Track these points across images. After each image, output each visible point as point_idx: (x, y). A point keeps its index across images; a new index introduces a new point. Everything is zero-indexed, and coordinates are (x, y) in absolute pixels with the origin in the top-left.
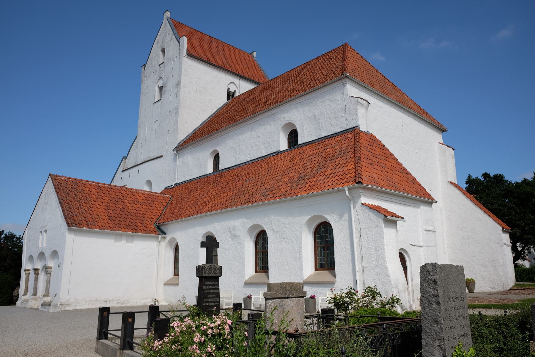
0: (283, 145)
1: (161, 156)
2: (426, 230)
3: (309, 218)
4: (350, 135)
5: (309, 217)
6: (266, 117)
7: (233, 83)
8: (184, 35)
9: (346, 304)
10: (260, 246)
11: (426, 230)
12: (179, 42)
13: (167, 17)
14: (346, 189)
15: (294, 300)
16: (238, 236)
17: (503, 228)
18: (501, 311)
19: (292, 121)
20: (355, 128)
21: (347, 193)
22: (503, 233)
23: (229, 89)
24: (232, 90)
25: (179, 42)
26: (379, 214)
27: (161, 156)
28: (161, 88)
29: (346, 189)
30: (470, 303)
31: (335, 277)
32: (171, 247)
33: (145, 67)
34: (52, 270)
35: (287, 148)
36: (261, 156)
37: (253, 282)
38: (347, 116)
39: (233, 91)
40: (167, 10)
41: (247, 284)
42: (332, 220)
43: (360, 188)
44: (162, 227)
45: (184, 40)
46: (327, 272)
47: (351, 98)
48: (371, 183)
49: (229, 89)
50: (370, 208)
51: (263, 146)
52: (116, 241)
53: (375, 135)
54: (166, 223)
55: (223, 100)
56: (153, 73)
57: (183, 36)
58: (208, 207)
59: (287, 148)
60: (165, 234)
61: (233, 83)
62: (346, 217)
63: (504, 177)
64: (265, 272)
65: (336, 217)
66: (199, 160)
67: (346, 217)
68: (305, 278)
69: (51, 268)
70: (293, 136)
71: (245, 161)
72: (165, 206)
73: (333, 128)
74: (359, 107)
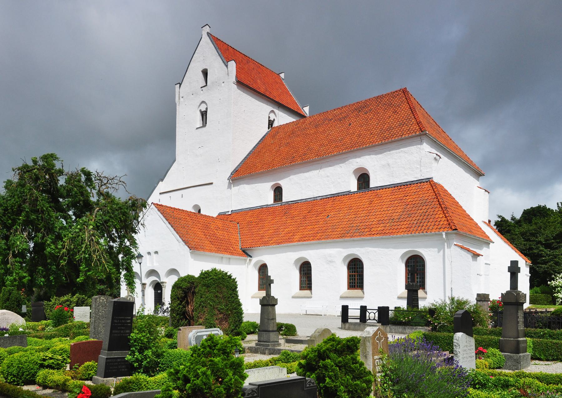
0: (353, 186)
1: (212, 183)
2: (486, 264)
3: (405, 251)
5: (405, 250)
6: (337, 160)
8: (233, 60)
11: (486, 264)
12: (227, 66)
14: (444, 233)
15: (13, 314)
16: (334, 262)
17: (526, 262)
19: (365, 166)
20: (430, 179)
21: (444, 236)
22: (473, 261)
24: (272, 119)
25: (227, 66)
26: (469, 252)
27: (212, 183)
28: (204, 114)
29: (444, 233)
31: (427, 294)
32: (256, 268)
33: (180, 86)
34: (166, 284)
35: (356, 190)
36: (330, 194)
37: (348, 296)
38: (422, 168)
39: (272, 120)
40: (207, 25)
41: (342, 298)
43: (456, 234)
44: (247, 252)
45: (232, 65)
46: (360, 290)
47: (426, 153)
49: (269, 117)
50: (462, 248)
51: (332, 185)
52: (194, 260)
53: (443, 186)
54: (254, 248)
55: (265, 130)
56: (193, 94)
57: (232, 60)
59: (356, 190)
60: (251, 257)
62: (442, 252)
64: (361, 289)
66: (259, 191)
67: (442, 252)
68: (399, 295)
69: (166, 283)
71: (312, 197)
73: (407, 177)
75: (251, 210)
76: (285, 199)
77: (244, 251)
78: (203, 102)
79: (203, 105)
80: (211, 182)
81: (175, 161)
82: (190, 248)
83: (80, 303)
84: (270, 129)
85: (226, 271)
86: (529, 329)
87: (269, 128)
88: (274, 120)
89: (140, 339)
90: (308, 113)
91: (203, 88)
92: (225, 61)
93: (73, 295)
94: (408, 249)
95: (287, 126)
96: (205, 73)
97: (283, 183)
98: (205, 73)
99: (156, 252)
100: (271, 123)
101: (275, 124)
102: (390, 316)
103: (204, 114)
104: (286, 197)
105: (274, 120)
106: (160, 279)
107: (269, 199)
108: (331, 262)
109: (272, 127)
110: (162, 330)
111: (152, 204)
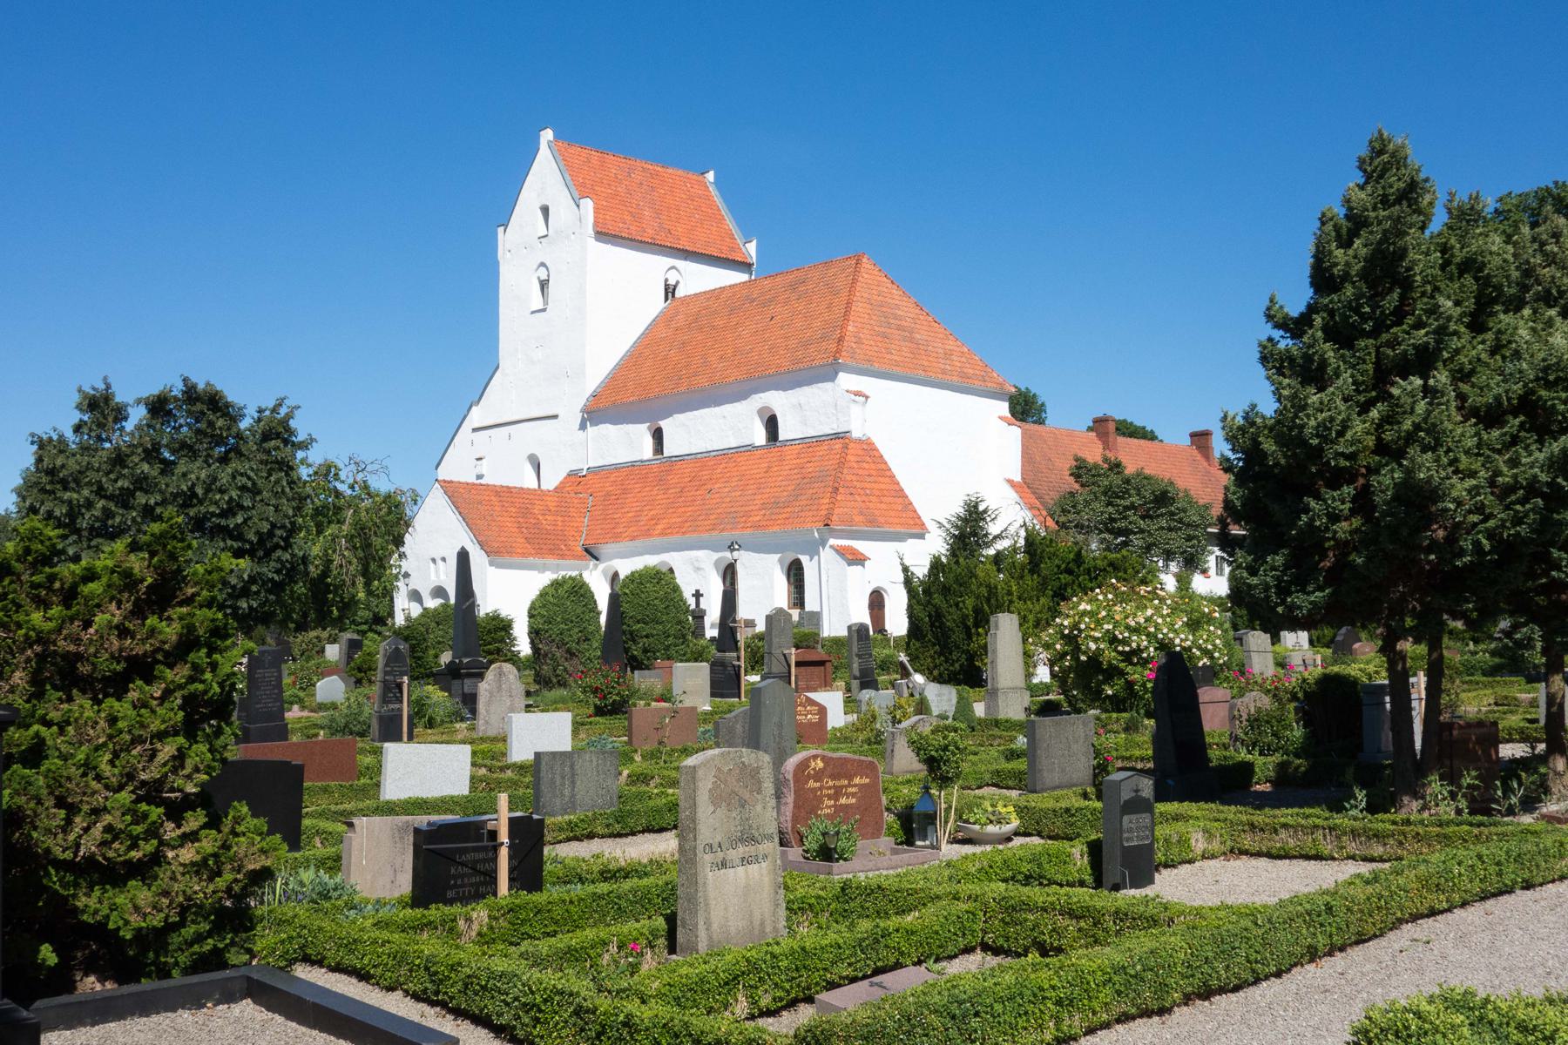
0: (759, 436)
1: (555, 417)
4: (838, 445)
7: (673, 268)
9: (1035, 681)
10: (728, 583)
13: (549, 142)
18: (1281, 664)
23: (666, 280)
24: (672, 282)
27: (555, 417)
28: (544, 285)
30: (795, 630)
42: (804, 559)
45: (588, 205)
48: (842, 522)
49: (666, 280)
55: (657, 304)
58: (660, 527)
60: (597, 559)
61: (673, 268)
63: (959, 517)
65: (808, 557)
67: (816, 558)
70: (772, 424)
74: (853, 406)
75: (617, 468)
76: (666, 453)
77: (587, 550)
78: (543, 264)
79: (543, 269)
81: (497, 367)
82: (488, 554)
83: (333, 640)
87: (666, 299)
88: (678, 282)
89: (726, 1006)
90: (754, 254)
92: (576, 195)
93: (324, 629)
96: (545, 210)
97: (663, 424)
98: (545, 210)
100: (670, 291)
101: (680, 293)
104: (670, 449)
105: (678, 282)
108: (699, 569)
109: (673, 296)
110: (312, 615)
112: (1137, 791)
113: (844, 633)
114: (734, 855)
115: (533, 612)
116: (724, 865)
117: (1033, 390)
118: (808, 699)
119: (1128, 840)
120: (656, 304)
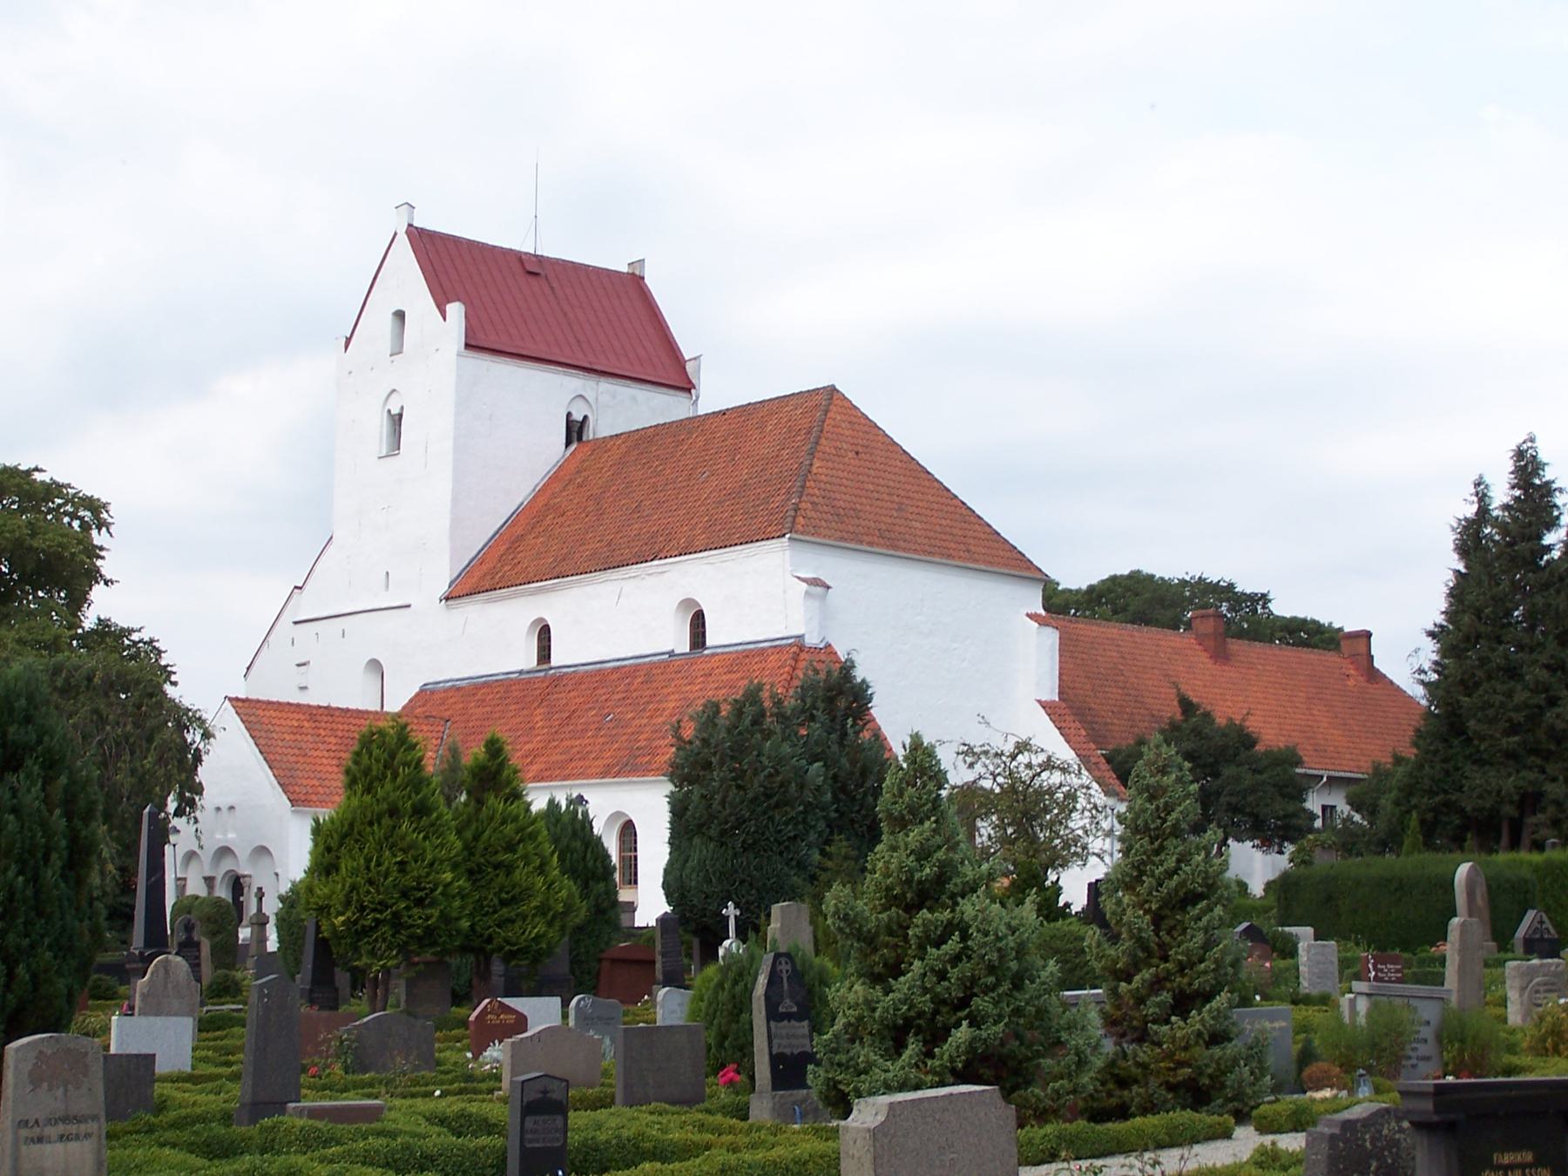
1: (408, 606)
23: (569, 415)
27: (408, 606)
39: (581, 419)
45: (456, 310)
58: (535, 767)
72: (439, 741)
76: (555, 661)
80: (406, 603)
82: (293, 802)
84: (573, 447)
85: (1450, 576)
86: (1137, 978)
87: (568, 444)
88: (585, 417)
91: (393, 358)
94: (172, 913)
95: (262, 742)
96: (400, 316)
98: (400, 316)
99: (232, 808)
100: (575, 430)
101: (589, 434)
102: (240, 942)
103: (396, 420)
106: (238, 866)
107: (523, 658)
109: (580, 439)
111: (227, 701)
112: (545, 1092)
113: (653, 923)
114: (52, 1131)
115: (1272, 885)
116: (40, 1140)
117: (1452, 546)
118: (503, 1006)
119: (530, 1141)
120: (552, 448)
